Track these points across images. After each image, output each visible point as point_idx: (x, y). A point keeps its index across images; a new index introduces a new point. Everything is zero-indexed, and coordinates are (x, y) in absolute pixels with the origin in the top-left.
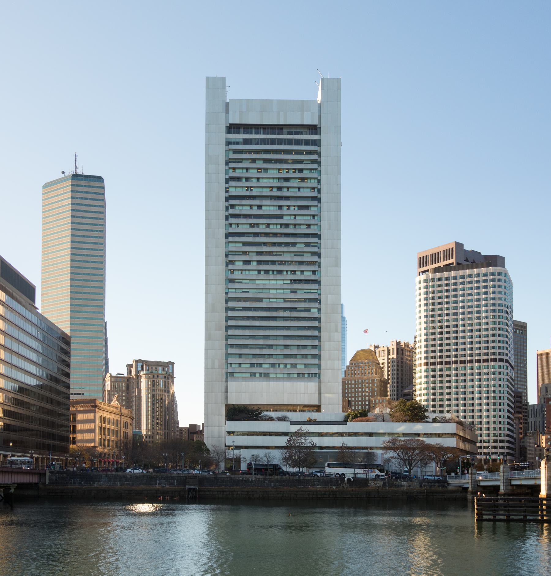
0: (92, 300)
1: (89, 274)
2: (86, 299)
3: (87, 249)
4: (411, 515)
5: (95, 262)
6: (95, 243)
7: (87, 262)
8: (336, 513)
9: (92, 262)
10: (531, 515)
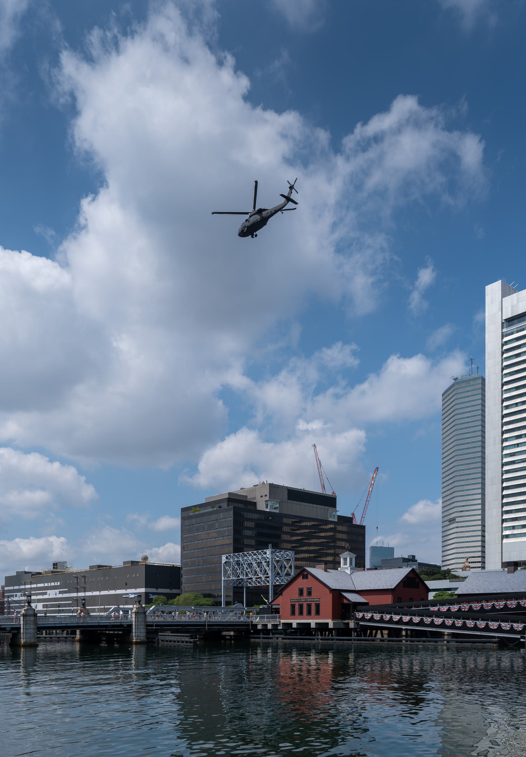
0: (472, 479)
1: (470, 458)
2: (468, 480)
3: (468, 438)
4: (21, 633)
5: (474, 447)
6: (474, 432)
7: (468, 448)
8: (189, 636)
9: (472, 448)
10: (304, 637)
